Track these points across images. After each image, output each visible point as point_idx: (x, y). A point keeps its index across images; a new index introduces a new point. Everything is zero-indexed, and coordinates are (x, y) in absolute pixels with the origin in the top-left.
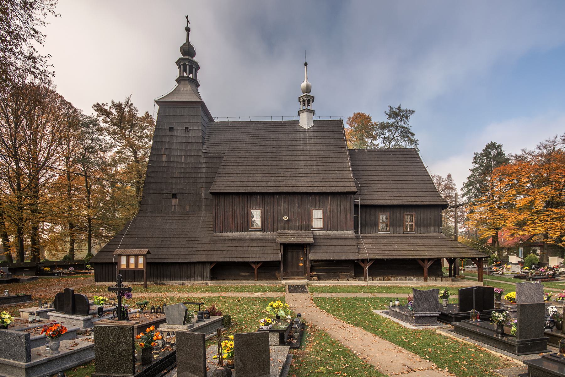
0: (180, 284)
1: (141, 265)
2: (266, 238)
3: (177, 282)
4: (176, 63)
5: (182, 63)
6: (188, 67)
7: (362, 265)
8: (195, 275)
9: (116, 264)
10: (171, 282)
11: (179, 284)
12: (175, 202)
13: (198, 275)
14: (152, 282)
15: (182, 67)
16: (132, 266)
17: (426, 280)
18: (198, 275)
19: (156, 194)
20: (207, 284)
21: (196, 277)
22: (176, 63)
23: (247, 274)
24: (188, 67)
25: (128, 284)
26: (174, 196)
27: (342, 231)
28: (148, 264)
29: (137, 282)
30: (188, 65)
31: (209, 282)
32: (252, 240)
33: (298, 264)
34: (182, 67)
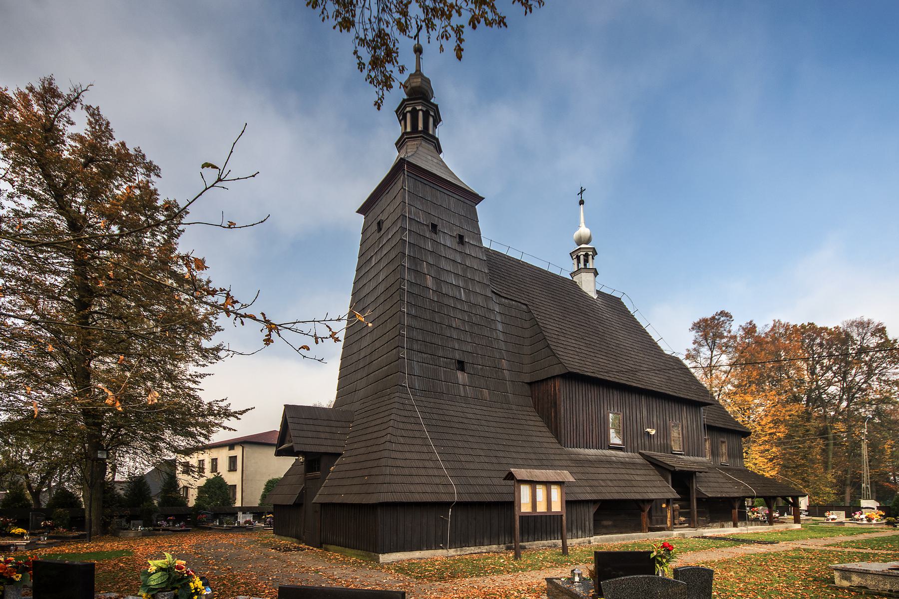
0: (551, 547)
1: (557, 507)
2: (611, 459)
3: (545, 542)
4: (287, 407)
5: (409, 109)
6: (421, 113)
7: (642, 505)
8: (573, 528)
9: (510, 505)
10: (536, 542)
11: (548, 547)
12: (461, 376)
13: (577, 529)
14: (501, 546)
15: (408, 115)
16: (541, 508)
17: (735, 525)
18: (577, 529)
19: (426, 355)
20: (590, 542)
21: (574, 531)
22: (287, 407)
23: (610, 523)
24: (421, 113)
25: (454, 554)
26: (461, 365)
27: (697, 458)
28: (569, 504)
29: (473, 548)
30: (421, 110)
31: (592, 539)
32: (608, 462)
33: (661, 505)
34: (408, 115)
